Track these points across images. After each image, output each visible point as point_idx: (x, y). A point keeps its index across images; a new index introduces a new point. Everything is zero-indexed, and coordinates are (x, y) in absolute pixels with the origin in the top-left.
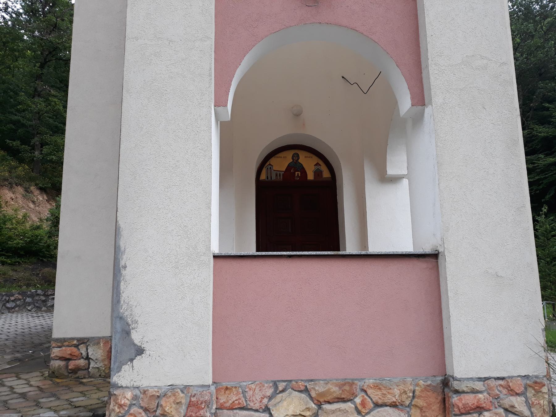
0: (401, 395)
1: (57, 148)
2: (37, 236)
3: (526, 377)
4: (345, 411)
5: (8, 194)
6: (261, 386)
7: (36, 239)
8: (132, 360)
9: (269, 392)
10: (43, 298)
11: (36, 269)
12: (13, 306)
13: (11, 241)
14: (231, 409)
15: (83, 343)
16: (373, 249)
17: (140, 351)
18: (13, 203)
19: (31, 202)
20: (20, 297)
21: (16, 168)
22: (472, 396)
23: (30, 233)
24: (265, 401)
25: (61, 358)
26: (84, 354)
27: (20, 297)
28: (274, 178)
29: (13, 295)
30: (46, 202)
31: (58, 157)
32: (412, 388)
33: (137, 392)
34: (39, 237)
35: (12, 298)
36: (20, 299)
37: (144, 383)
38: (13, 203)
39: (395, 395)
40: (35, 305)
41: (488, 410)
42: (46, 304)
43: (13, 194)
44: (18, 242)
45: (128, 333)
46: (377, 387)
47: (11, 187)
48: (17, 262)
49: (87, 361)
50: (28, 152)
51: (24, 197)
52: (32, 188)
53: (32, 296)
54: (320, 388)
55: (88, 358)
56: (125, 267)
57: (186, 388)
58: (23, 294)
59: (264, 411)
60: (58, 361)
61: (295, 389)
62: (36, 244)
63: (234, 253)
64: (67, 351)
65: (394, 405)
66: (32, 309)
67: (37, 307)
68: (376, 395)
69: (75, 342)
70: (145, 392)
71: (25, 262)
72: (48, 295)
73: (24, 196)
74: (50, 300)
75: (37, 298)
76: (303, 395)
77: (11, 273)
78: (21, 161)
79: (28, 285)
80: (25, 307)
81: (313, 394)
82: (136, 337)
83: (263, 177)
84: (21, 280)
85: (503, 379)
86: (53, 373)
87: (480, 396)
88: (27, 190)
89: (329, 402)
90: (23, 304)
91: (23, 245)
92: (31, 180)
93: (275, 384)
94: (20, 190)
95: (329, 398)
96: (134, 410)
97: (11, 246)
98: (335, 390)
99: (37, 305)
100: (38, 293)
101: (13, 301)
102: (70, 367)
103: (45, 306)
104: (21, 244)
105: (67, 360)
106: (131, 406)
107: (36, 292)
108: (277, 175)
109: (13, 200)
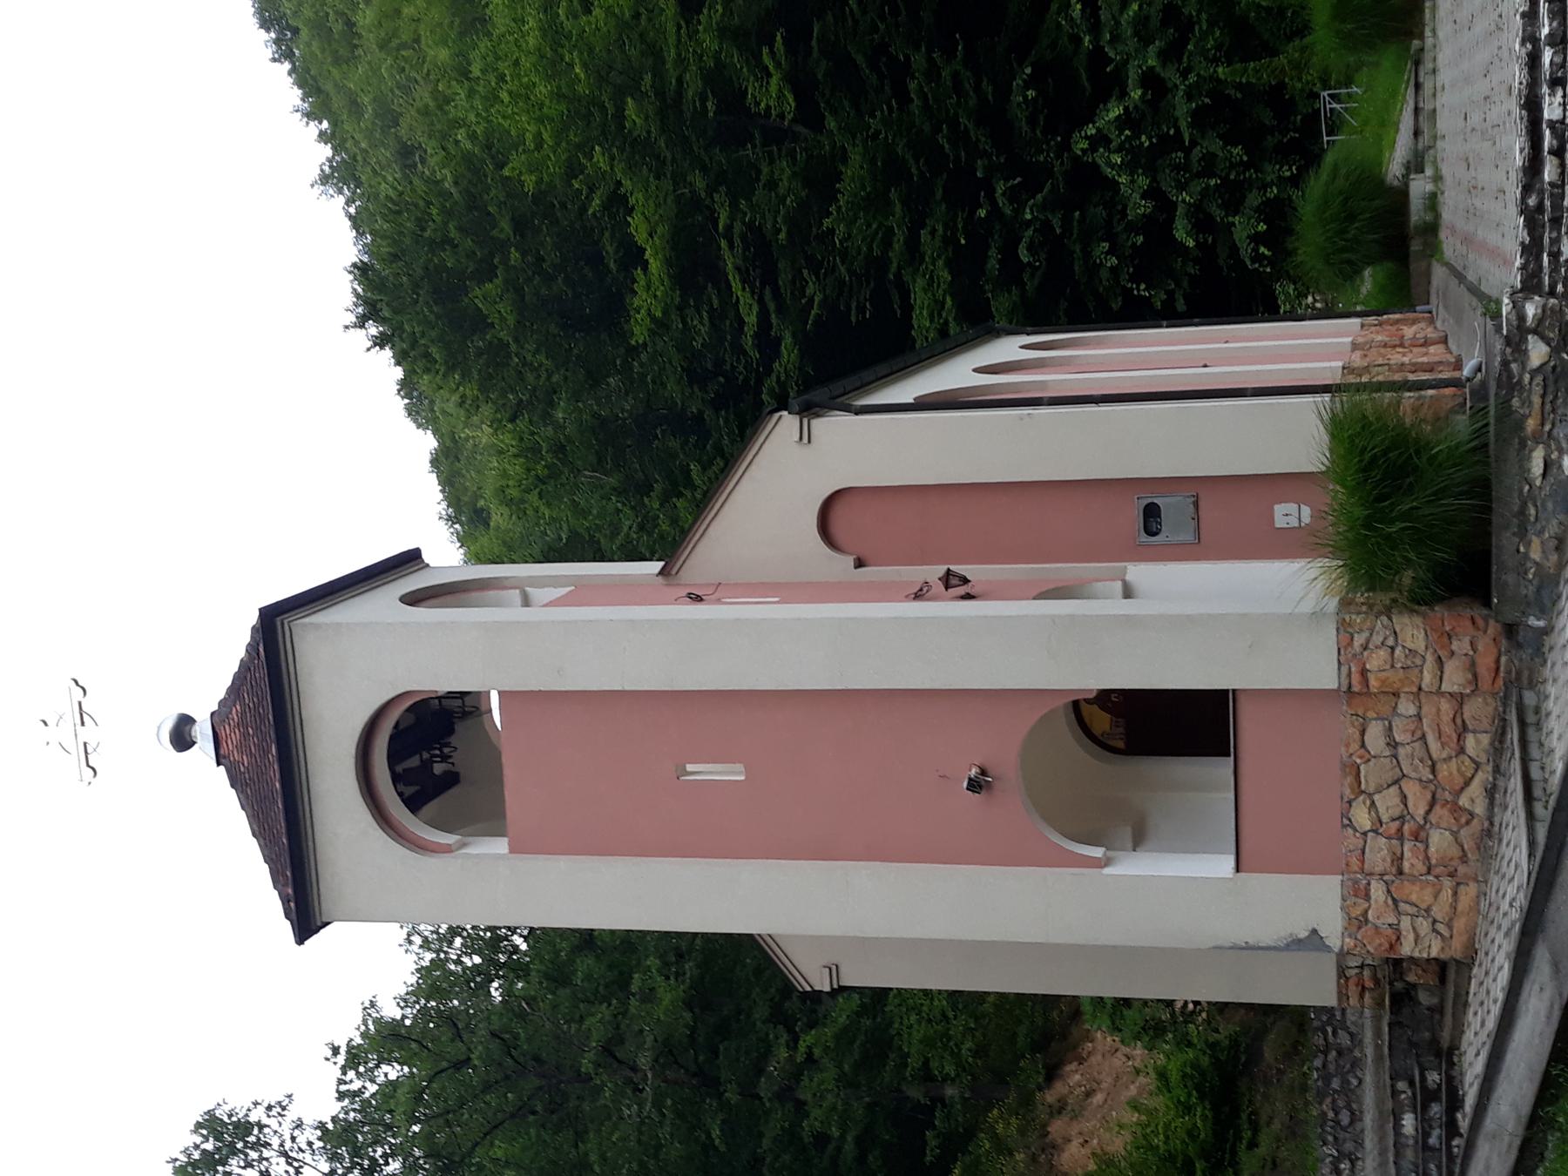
1: (941, 1041)
2: (1185, 1076)
3: (1338, 629)
4: (1367, 772)
5: (1073, 1154)
7: (1192, 1077)
8: (1322, 938)
9: (1350, 831)
15: (1343, 972)
19: (1090, 1100)
20: (1329, 1100)
22: (1353, 676)
25: (1362, 996)
26: (1357, 971)
27: (1329, 1100)
28: (1121, 730)
29: (1324, 1114)
30: (1086, 1064)
33: (1346, 934)
34: (1188, 1070)
35: (1331, 1115)
36: (1334, 1101)
37: (1339, 929)
38: (1095, 1141)
40: (1349, 1072)
41: (1364, 664)
44: (1200, 1118)
45: (1300, 941)
46: (1347, 745)
51: (1075, 1117)
53: (1327, 1079)
54: (1348, 792)
55: (1362, 967)
56: (1246, 943)
58: (1321, 1096)
61: (90, 764)
64: (1353, 990)
65: (1363, 733)
66: (1356, 1077)
68: (1355, 746)
69: (1342, 981)
74: (1339, 1041)
75: (1332, 1068)
76: (1354, 804)
77: (1277, 1125)
80: (1352, 1091)
82: (1303, 934)
83: (1120, 744)
84: (1293, 1106)
85: (1339, 649)
87: (1353, 669)
88: (1059, 1109)
91: (1208, 1107)
92: (1027, 1101)
93: (1344, 826)
94: (1057, 1127)
95: (1356, 785)
96: (1359, 937)
98: (1349, 779)
99: (1348, 1066)
101: (1337, 1114)
103: (1352, 1051)
106: (1356, 939)
107: (1317, 1069)
108: (1118, 726)
109: (1086, 1141)
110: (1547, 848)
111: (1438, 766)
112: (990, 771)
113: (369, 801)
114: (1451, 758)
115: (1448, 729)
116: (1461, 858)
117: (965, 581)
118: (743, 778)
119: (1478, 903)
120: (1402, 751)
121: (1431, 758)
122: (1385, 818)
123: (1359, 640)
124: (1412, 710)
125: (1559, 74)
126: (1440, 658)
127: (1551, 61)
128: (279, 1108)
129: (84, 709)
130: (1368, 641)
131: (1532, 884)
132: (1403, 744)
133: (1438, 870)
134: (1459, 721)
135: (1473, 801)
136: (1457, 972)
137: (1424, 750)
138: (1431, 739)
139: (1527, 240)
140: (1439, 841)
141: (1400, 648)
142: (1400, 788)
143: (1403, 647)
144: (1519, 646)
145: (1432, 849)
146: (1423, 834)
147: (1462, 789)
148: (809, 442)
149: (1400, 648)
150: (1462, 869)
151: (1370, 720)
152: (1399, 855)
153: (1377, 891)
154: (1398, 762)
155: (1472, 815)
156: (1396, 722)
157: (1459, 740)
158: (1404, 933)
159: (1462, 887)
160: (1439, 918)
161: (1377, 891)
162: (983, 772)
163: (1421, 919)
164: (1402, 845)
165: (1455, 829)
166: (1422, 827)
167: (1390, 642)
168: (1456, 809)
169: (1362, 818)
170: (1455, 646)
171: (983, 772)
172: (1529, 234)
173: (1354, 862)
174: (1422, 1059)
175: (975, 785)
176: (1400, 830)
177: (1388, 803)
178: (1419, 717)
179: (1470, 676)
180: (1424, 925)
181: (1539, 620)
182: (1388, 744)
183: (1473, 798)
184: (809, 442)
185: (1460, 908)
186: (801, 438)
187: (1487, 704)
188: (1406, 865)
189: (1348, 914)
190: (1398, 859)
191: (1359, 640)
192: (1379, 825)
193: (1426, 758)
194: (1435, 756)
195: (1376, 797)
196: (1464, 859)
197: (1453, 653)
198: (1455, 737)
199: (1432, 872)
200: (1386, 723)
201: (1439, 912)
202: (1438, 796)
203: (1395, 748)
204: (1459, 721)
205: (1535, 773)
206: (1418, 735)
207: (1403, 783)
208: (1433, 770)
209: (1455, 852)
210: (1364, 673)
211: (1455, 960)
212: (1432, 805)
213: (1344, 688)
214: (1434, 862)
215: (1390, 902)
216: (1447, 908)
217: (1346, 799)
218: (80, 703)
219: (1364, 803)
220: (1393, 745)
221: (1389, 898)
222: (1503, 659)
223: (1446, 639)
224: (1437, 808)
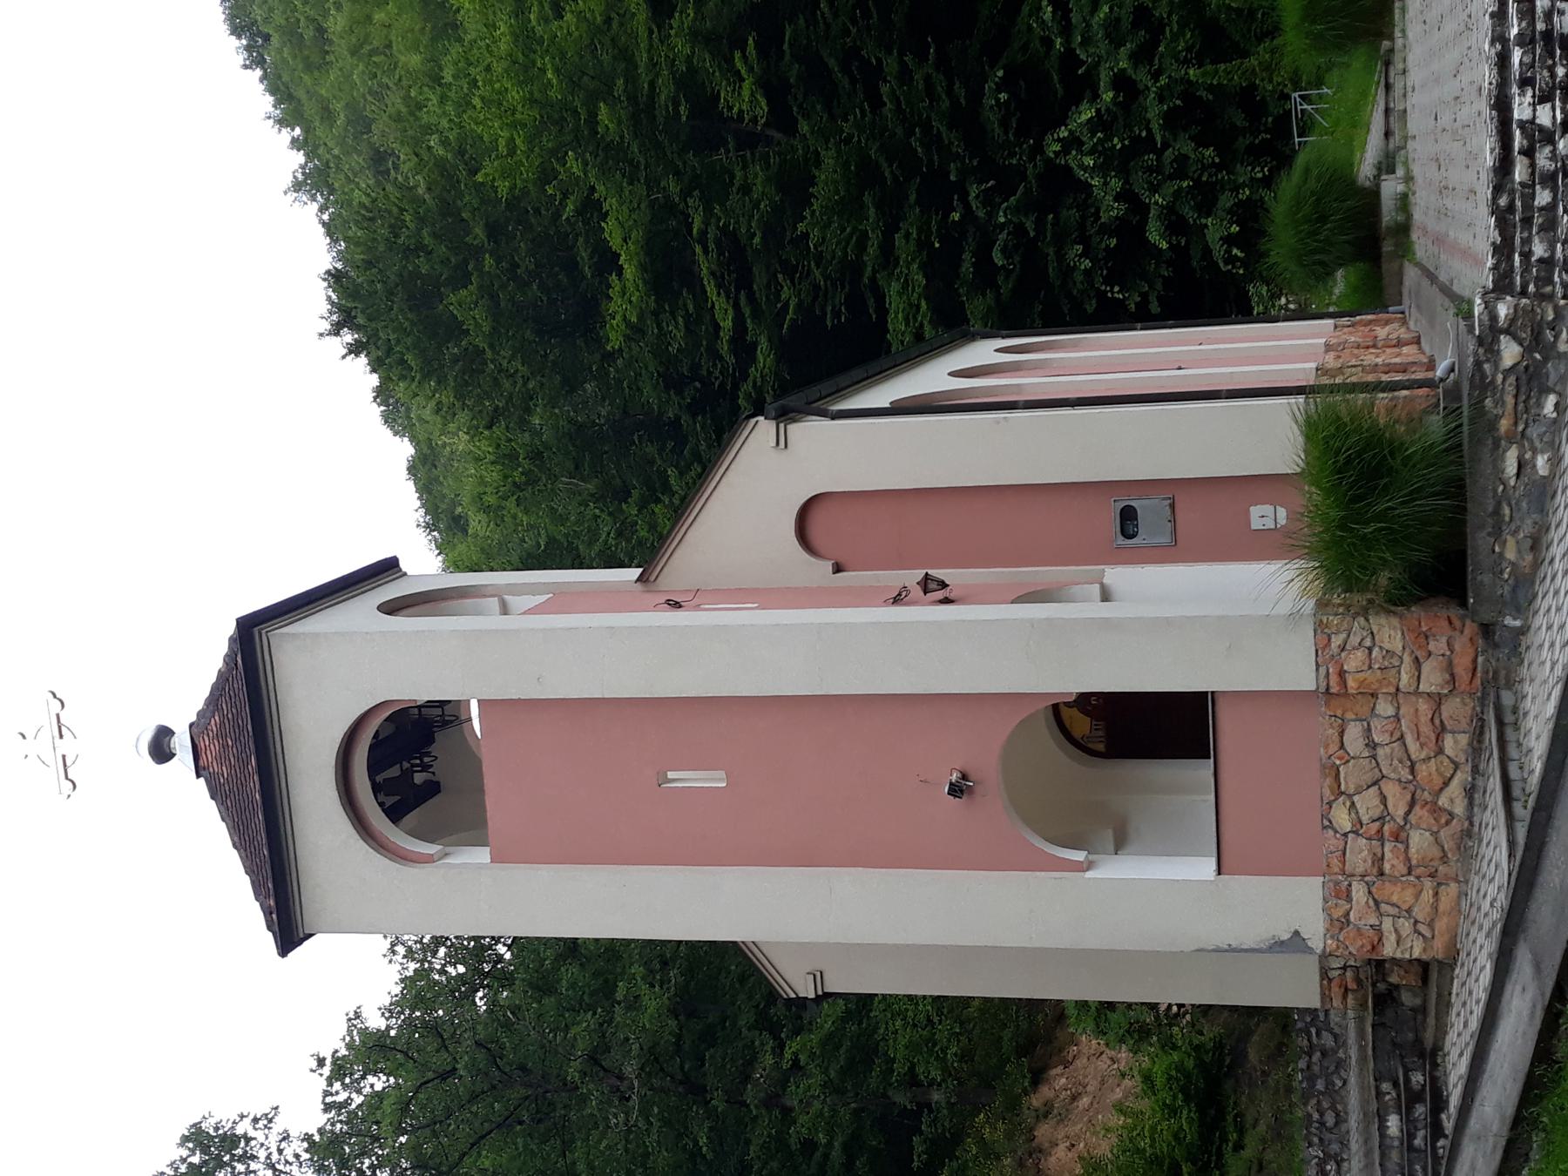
0: (1333, 728)
2: (1170, 1078)
3: (1315, 631)
7: (1178, 1080)
8: (1304, 940)
9: (1331, 832)
10: (1317, 1056)
11: (1250, 1078)
12: (1334, 1115)
13: (1185, 1137)
14: (1344, 863)
17: (1297, 933)
18: (1082, 1145)
20: (1314, 1101)
21: (981, 1142)
22: (1331, 677)
23: (1163, 1094)
24: (1338, 835)
25: (1345, 997)
26: (1339, 972)
27: (1314, 1101)
28: (1101, 733)
29: (1310, 1116)
31: (950, 1041)
32: (1327, 717)
33: (1328, 936)
35: (1316, 1116)
37: (1322, 930)
38: (1082, 1145)
39: (1333, 733)
40: (1332, 1073)
41: (1342, 665)
42: (1332, 1049)
43: (1057, 1145)
44: (1186, 1120)
45: (1282, 942)
46: (1326, 747)
47: (1040, 1152)
48: (1235, 1121)
49: (1349, 969)
50: (936, 1117)
52: (1036, 1101)
53: (1312, 1079)
54: (1327, 792)
55: (1344, 968)
56: (1230, 945)
57: (1325, 900)
59: (1347, 837)
60: (1348, 1001)
61: (70, 777)
62: (1188, 1076)
63: (1212, 797)
64: (1336, 992)
66: (1341, 1078)
67: (1336, 1067)
68: (1334, 748)
69: (1325, 982)
70: (1328, 930)
71: (1235, 1103)
72: (1311, 1047)
73: (1062, 1120)
75: (1316, 1069)
76: (1334, 805)
77: (1262, 1127)
78: (957, 1138)
79: (1289, 1090)
81: (1333, 798)
82: (1286, 936)
83: (1101, 747)
84: (1278, 1107)
85: (1317, 651)
86: (1361, 1005)
87: (1331, 670)
88: (1045, 1113)
89: (1339, 786)
90: (1330, 1096)
92: (1013, 1105)
93: (1325, 828)
94: (1043, 1131)
95: (1336, 787)
97: (1196, 1136)
98: (1328, 781)
99: (1332, 1068)
100: (1305, 1067)
101: (1322, 1115)
102: (1355, 987)
104: (1192, 1115)
105: (1346, 990)
106: (1338, 940)
107: (1302, 1070)
109: (1073, 1145)
110: (1527, 847)
111: (1417, 766)
112: (972, 775)
113: (352, 815)
115: (1426, 729)
118: (724, 785)
119: (1459, 904)
120: (1380, 752)
121: (1410, 759)
122: (1365, 819)
123: (1337, 641)
124: (1390, 711)
125: (1529, 74)
126: (1417, 658)
134: (1437, 722)
138: (1409, 739)
139: (1499, 240)
140: (1419, 841)
142: (1380, 788)
143: (1381, 647)
144: (1496, 646)
145: (1413, 850)
146: (1403, 835)
147: (1441, 789)
148: (786, 446)
151: (1349, 721)
152: (1379, 855)
153: (1359, 892)
155: (1451, 814)
157: (1437, 742)
158: (1386, 934)
159: (1443, 887)
160: (1420, 918)
161: (1359, 892)
162: (964, 777)
164: (1383, 845)
168: (1436, 810)
172: (1500, 235)
175: (956, 790)
176: (1380, 831)
177: (1368, 804)
178: (1397, 718)
180: (1406, 926)
181: (1515, 619)
183: (1453, 798)
184: (786, 446)
185: (1441, 908)
187: (1465, 704)
188: (1387, 867)
191: (1337, 641)
192: (1358, 826)
195: (1356, 798)
196: (1444, 858)
197: (1430, 654)
200: (1365, 724)
202: (1417, 797)
203: (1374, 749)
204: (1437, 722)
206: (1397, 735)
208: (1412, 770)
209: (1437, 853)
210: (1342, 674)
213: (1322, 689)
214: (1414, 862)
215: (1371, 903)
216: (1428, 909)
218: (58, 716)
220: (1372, 745)
222: (1480, 659)
223: (1422, 640)
224: (1417, 808)
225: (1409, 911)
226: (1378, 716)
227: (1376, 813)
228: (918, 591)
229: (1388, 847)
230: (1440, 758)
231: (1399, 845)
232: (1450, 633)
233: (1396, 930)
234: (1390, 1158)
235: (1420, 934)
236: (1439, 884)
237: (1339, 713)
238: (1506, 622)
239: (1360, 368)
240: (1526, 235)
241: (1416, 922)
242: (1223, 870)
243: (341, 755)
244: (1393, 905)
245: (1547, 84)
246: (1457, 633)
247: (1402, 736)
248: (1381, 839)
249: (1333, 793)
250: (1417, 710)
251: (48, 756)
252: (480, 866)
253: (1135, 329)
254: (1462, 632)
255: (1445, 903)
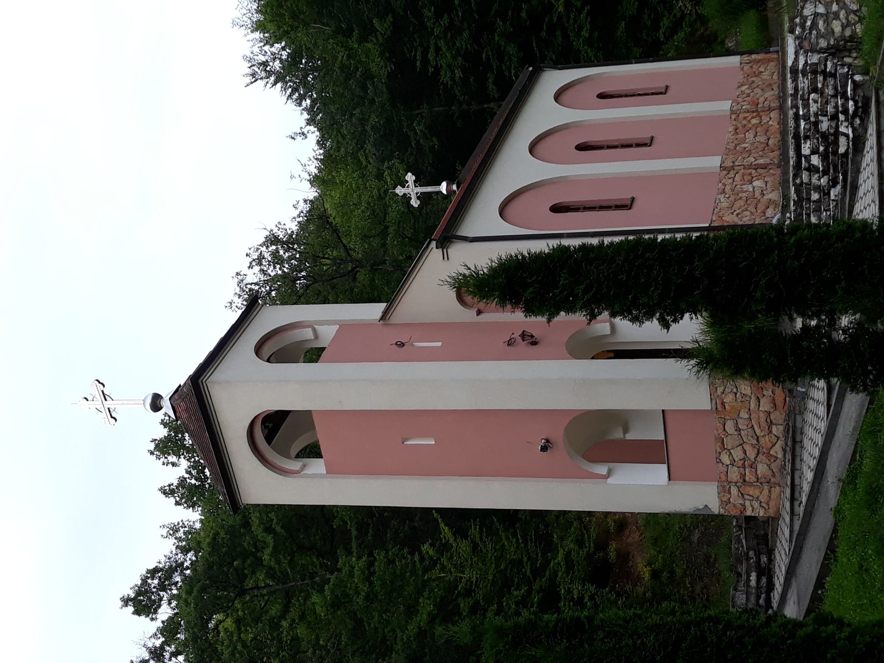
6: (718, 467)
16: (662, 438)
37: (718, 505)
45: (700, 509)
46: (717, 430)
54: (719, 450)
61: (113, 416)
68: (720, 431)
76: (722, 454)
85: (711, 394)
98: (719, 444)
106: (725, 509)
110: (798, 535)
111: (760, 438)
112: (551, 441)
113: (257, 454)
114: (766, 435)
115: (764, 424)
116: (772, 475)
117: (532, 336)
118: (434, 443)
119: (780, 495)
120: (742, 433)
121: (756, 435)
122: (736, 459)
123: (720, 390)
124: (747, 416)
125: (808, 134)
126: (758, 397)
127: (804, 127)
128: (177, 503)
129: (105, 393)
130: (724, 390)
131: (791, 552)
132: (743, 430)
133: (762, 480)
134: (769, 420)
135: (776, 453)
136: (772, 521)
137: (753, 432)
138: (756, 428)
139: (796, 199)
140: (762, 469)
141: (739, 393)
142: (743, 447)
143: (741, 393)
144: (794, 397)
145: (759, 472)
146: (754, 466)
147: (771, 448)
148: (448, 259)
149: (739, 393)
150: (773, 480)
151: (727, 419)
152: (744, 474)
153: (734, 491)
154: (741, 437)
155: (777, 458)
156: (740, 421)
157: (769, 429)
158: (747, 507)
159: (773, 489)
160: (762, 500)
161: (734, 491)
162: (548, 441)
163: (754, 502)
164: (745, 470)
165: (769, 463)
166: (754, 463)
167: (735, 390)
168: (769, 455)
169: (726, 459)
170: (765, 392)
171: (548, 441)
172: (797, 196)
173: (724, 478)
174: (760, 547)
175: (544, 449)
176: (744, 464)
177: (738, 454)
178: (750, 418)
179: (772, 405)
180: (756, 504)
181: (802, 388)
182: (736, 430)
183: (777, 451)
184: (448, 259)
185: (772, 497)
186: (444, 258)
187: (781, 414)
188: (747, 479)
189: (721, 499)
190: (743, 476)
191: (720, 390)
192: (733, 462)
193: (754, 435)
194: (758, 435)
195: (732, 451)
196: (774, 475)
197: (764, 395)
198: (767, 428)
199: (759, 481)
200: (735, 421)
201: (762, 499)
202: (760, 450)
203: (740, 431)
204: (769, 420)
205: (797, 482)
206: (750, 426)
207: (744, 445)
208: (758, 441)
209: (770, 473)
210: (723, 404)
211: (771, 517)
212: (758, 454)
213: (714, 409)
214: (760, 476)
215: (740, 494)
216: (766, 497)
217: (718, 452)
218: (103, 391)
219: (726, 453)
220: (738, 430)
221: (740, 494)
222: (787, 399)
223: (760, 390)
224: (760, 455)
225: (757, 498)
226: (741, 418)
227: (742, 456)
228: (520, 339)
229: (747, 470)
230: (770, 435)
231: (753, 470)
232: (773, 387)
233: (752, 506)
234: (750, 601)
235: (763, 507)
236: (771, 487)
237: (723, 417)
238: (798, 389)
239: (743, 167)
240: (808, 206)
241: (761, 502)
242: (671, 477)
243: (249, 435)
244: (750, 495)
245: (816, 146)
246: (776, 388)
247: (752, 426)
248: (744, 467)
249: (720, 448)
250: (759, 416)
251: (100, 407)
252: (320, 476)
253: (631, 63)
254: (779, 387)
255: (774, 496)
